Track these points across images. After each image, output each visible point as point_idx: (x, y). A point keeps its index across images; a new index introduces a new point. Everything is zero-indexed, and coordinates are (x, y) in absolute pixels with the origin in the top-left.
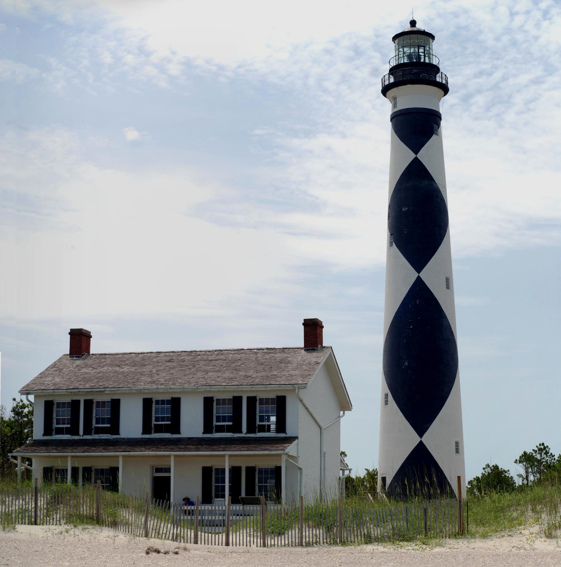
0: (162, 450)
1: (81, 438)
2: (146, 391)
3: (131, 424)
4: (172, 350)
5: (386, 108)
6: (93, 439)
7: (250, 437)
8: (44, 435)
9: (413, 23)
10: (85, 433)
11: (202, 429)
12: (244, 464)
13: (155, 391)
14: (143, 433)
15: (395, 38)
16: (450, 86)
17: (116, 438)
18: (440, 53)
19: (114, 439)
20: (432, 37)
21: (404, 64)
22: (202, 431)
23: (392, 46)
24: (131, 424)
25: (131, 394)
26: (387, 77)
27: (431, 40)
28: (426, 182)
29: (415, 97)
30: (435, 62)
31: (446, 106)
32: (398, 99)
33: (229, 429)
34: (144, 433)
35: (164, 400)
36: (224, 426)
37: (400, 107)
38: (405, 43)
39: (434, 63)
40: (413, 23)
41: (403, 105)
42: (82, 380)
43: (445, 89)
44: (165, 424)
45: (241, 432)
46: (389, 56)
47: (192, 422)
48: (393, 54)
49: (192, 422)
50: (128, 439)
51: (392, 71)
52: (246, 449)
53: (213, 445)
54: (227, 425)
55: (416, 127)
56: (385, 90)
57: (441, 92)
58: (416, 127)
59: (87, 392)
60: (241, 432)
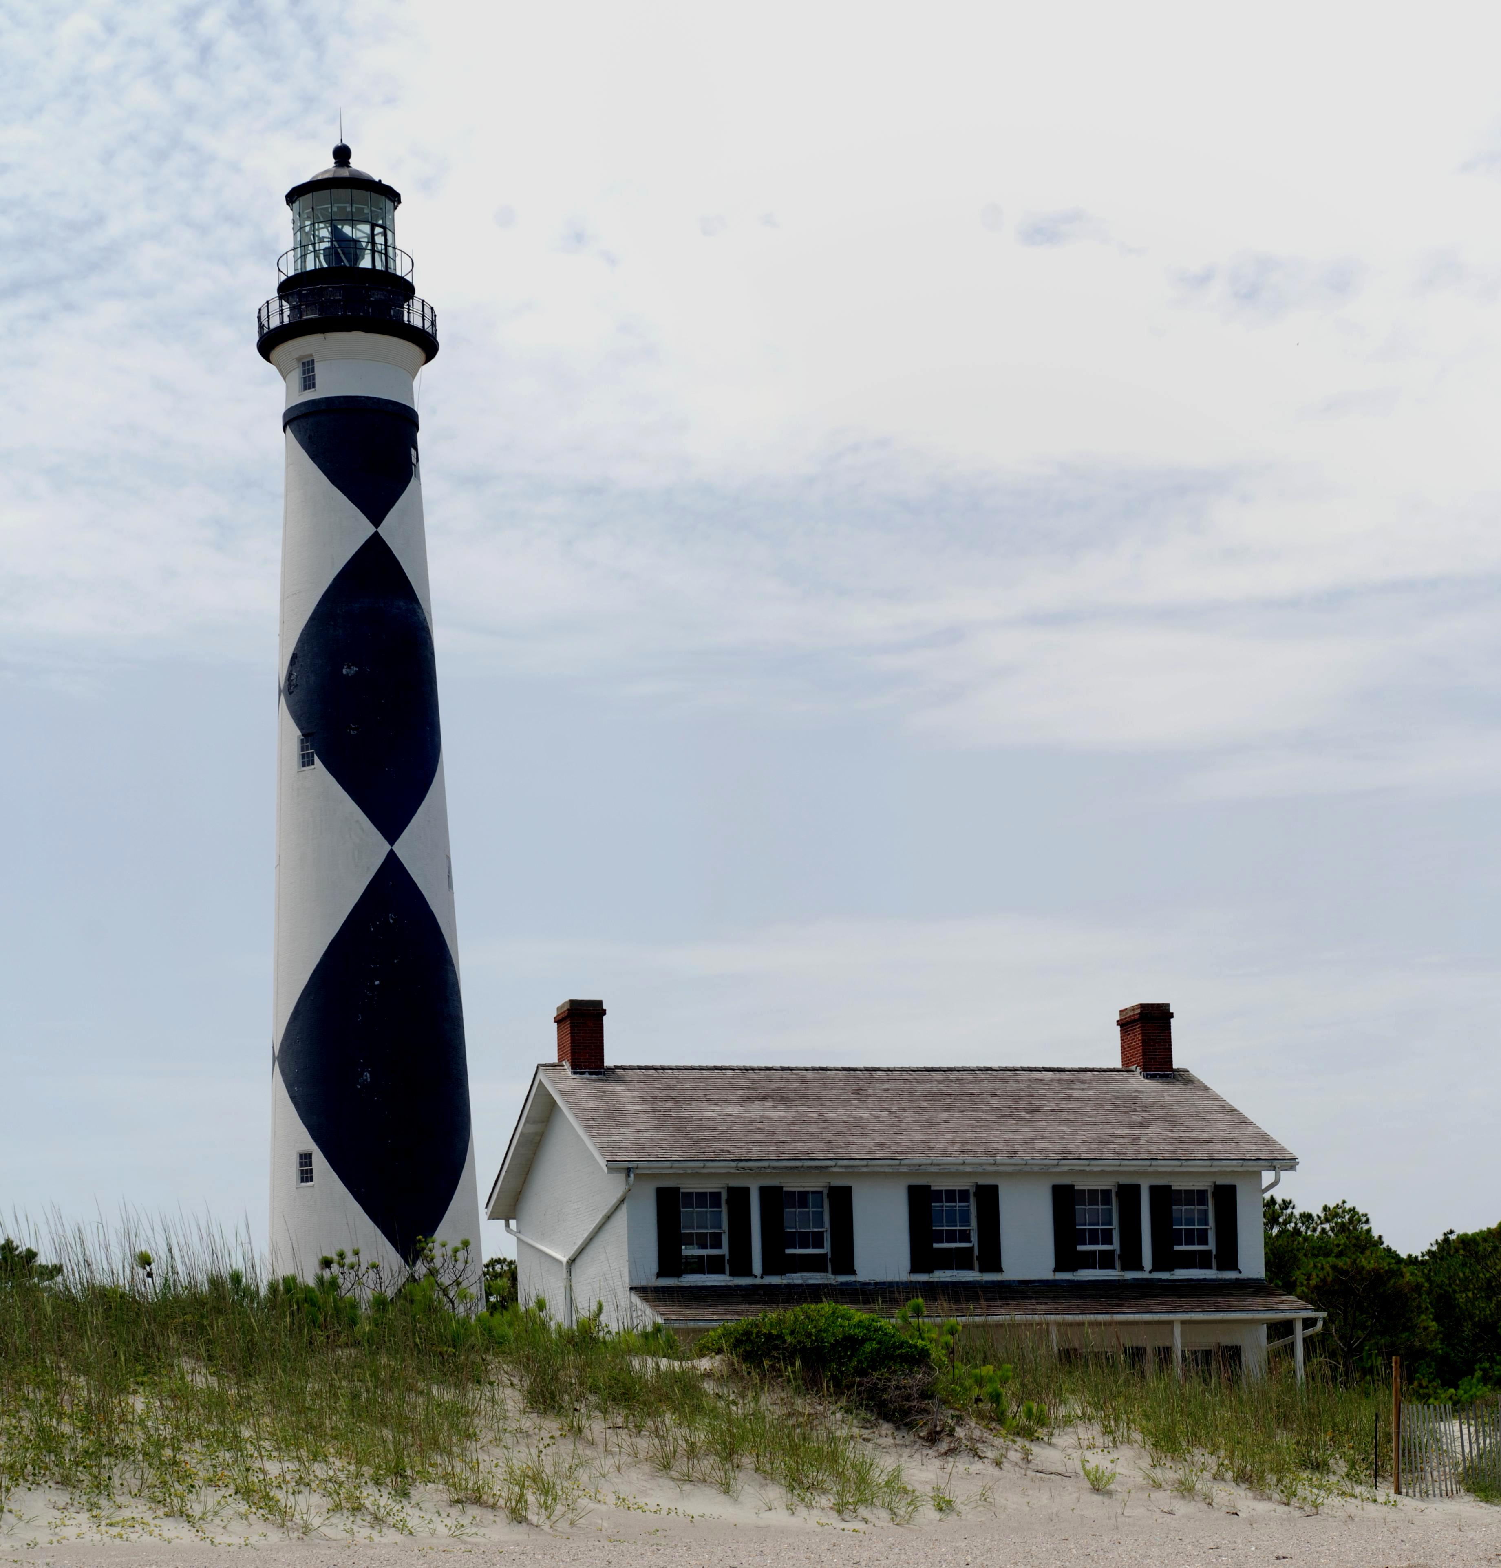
0: (1165, 1308)
1: (758, 1281)
2: (968, 1169)
3: (882, 1246)
4: (982, 1065)
5: (272, 392)
6: (788, 1286)
7: (1160, 1280)
8: (659, 1275)
9: (342, 154)
10: (766, 1272)
11: (1051, 1263)
12: (1287, 1343)
13: (953, 1169)
14: (1057, 1269)
15: (293, 196)
16: (441, 338)
17: (847, 1283)
18: (422, 247)
19: (842, 1284)
20: (394, 197)
21: (317, 273)
22: (1052, 1264)
23: (286, 214)
24: (882, 1246)
25: (875, 1173)
26: (275, 306)
27: (389, 204)
28: (401, 604)
29: (351, 366)
30: (401, 268)
31: (432, 392)
32: (317, 365)
33: (715, 1265)
34: (914, 1270)
35: (1193, 1191)
36: (1094, 1252)
37: (321, 392)
38: (335, 209)
39: (399, 273)
40: (342, 154)
41: (332, 383)
42: (1146, 1141)
43: (427, 344)
44: (957, 1249)
45: (1141, 1268)
46: (272, 247)
47: (1027, 1245)
48: (286, 238)
49: (1027, 1245)
50: (876, 1284)
51: (286, 289)
52: (1134, 1310)
53: (1143, 1296)
54: (1101, 1252)
55: (363, 449)
56: (268, 343)
57: (414, 351)
58: (363, 449)
59: (786, 1168)
60: (1141, 1268)
